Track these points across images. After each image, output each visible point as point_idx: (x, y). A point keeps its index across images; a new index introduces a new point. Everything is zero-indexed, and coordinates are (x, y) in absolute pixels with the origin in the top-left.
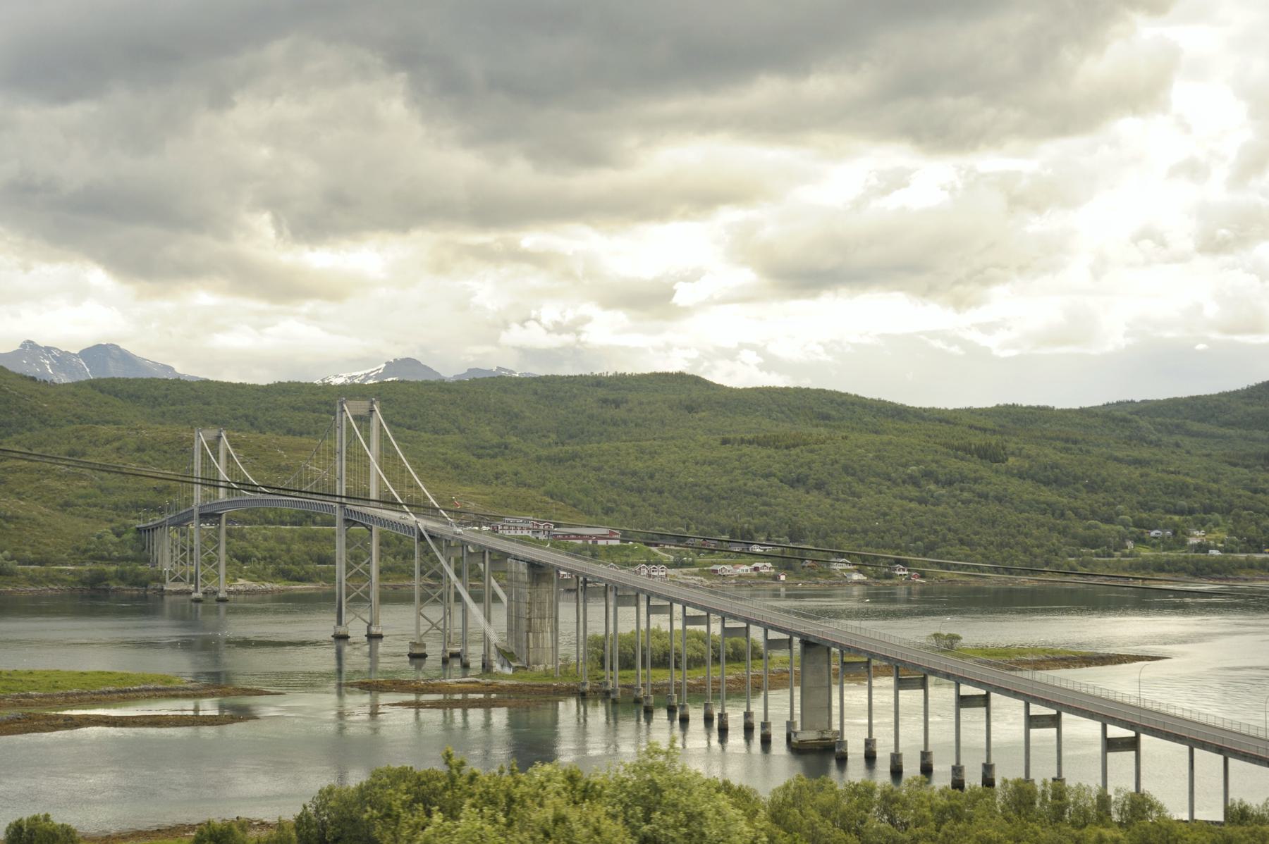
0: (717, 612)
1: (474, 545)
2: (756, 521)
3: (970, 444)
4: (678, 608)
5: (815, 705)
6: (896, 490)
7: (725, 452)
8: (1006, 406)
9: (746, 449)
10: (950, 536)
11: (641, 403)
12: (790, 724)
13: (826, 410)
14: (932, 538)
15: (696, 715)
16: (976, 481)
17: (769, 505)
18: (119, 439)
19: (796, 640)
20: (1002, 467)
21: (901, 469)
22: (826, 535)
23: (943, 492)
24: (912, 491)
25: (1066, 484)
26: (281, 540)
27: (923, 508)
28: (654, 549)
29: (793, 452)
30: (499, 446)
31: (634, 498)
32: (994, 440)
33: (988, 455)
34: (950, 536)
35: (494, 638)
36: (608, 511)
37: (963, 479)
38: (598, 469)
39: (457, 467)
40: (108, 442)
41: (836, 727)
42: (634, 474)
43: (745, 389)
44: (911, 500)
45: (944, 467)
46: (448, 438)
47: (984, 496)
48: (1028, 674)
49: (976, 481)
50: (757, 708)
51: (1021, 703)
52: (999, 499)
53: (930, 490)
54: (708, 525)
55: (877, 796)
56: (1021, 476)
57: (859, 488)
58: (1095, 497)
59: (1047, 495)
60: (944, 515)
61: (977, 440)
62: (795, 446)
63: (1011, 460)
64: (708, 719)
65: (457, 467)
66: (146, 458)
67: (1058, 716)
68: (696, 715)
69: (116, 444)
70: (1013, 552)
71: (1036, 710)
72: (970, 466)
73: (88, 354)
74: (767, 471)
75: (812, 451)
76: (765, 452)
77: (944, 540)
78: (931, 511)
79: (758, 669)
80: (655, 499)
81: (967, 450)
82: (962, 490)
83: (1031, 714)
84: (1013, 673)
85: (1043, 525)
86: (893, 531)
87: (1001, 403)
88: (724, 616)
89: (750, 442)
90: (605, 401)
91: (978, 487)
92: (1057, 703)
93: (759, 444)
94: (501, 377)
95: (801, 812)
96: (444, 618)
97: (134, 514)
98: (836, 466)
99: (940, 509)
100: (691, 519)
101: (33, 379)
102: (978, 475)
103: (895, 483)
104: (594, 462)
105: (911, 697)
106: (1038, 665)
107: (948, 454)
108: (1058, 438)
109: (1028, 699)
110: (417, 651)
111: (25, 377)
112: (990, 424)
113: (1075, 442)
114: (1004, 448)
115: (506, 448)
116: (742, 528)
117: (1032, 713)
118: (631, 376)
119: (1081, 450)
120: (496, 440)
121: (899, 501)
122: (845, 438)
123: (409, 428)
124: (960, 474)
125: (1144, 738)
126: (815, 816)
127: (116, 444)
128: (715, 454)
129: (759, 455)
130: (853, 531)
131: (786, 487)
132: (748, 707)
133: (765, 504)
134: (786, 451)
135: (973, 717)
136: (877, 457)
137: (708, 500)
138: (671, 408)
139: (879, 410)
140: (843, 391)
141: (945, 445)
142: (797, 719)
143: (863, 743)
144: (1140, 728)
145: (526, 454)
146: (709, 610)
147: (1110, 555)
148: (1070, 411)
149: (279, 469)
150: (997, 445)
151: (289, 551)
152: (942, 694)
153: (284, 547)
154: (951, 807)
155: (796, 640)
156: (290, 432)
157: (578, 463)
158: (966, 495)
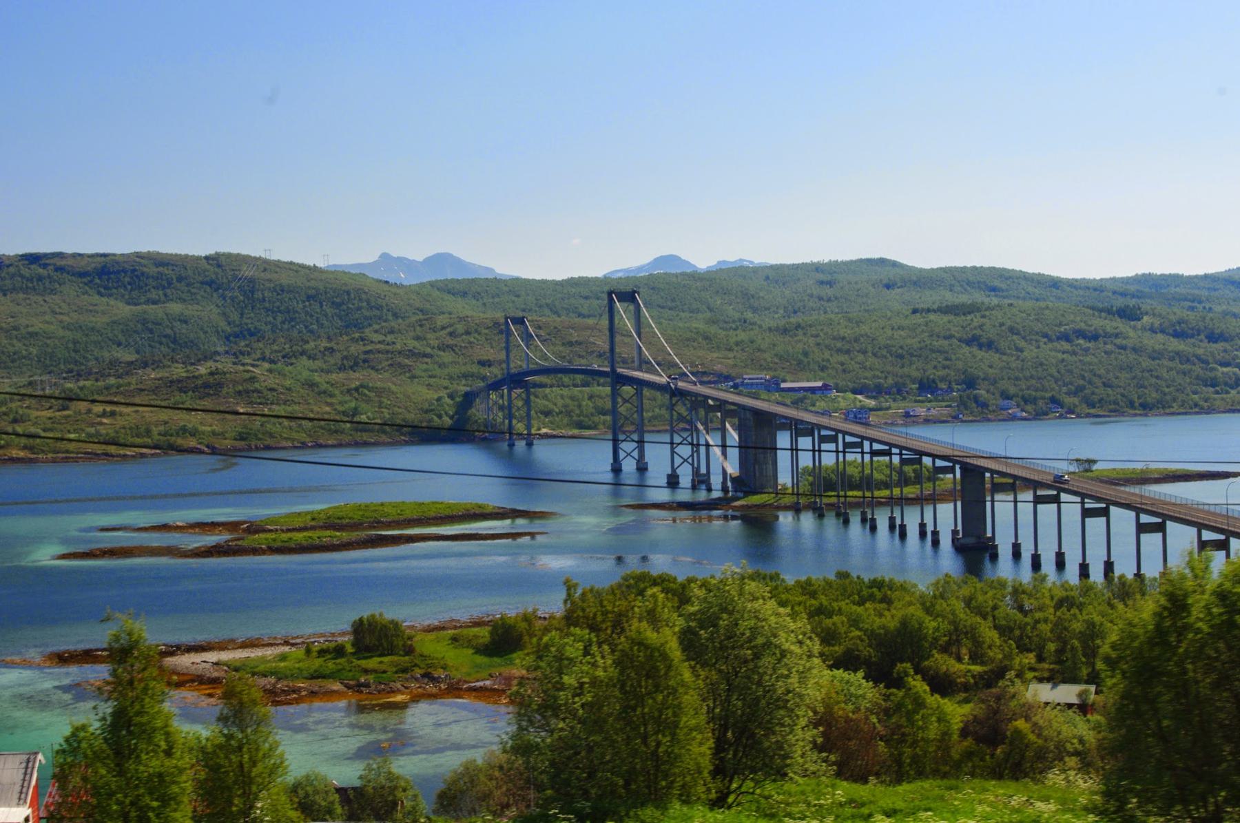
0: (896, 446)
1: (713, 399)
2: (940, 373)
3: (1112, 307)
4: (866, 444)
5: (974, 516)
6: (1050, 345)
7: (918, 319)
8: (1144, 275)
9: (932, 316)
10: (1095, 380)
11: (849, 283)
12: (955, 532)
13: (996, 283)
14: (1081, 382)
15: (855, 519)
16: (1117, 336)
17: (950, 360)
18: (451, 325)
19: (957, 467)
20: (1139, 324)
21: (1057, 328)
22: (996, 382)
23: (1088, 345)
24: (1066, 346)
25: (1192, 336)
26: (572, 398)
27: (1074, 358)
28: (859, 397)
29: (969, 317)
30: (740, 320)
31: (842, 358)
32: (1132, 302)
33: (1129, 314)
34: (1095, 380)
35: (730, 470)
36: (823, 369)
37: (1107, 335)
38: (817, 336)
39: (706, 338)
40: (443, 328)
41: (989, 534)
42: (843, 338)
43: (932, 269)
44: (1063, 353)
45: (1091, 326)
46: (700, 316)
47: (1124, 348)
48: (1135, 490)
49: (1117, 336)
50: (897, 514)
51: (1133, 514)
52: (1134, 350)
53: (1079, 344)
54: (901, 377)
55: (1010, 589)
56: (1152, 330)
57: (1022, 344)
58: (1215, 345)
59: (1175, 345)
60: (1090, 364)
61: (1119, 302)
62: (969, 313)
63: (1145, 318)
64: (864, 520)
65: (706, 338)
66: (472, 339)
67: (1058, 496)
68: (855, 519)
69: (449, 330)
70: (1146, 391)
71: (1145, 519)
72: (1119, 324)
73: (429, 261)
74: (948, 333)
75: (983, 317)
76: (946, 318)
77: (1090, 382)
78: (1080, 361)
79: (928, 488)
80: (860, 357)
81: (1109, 311)
82: (1105, 343)
83: (1203, 539)
84: (1118, 488)
85: (1171, 369)
86: (1049, 378)
87: (1140, 273)
88: (872, 440)
89: (935, 311)
90: (822, 283)
91: (1118, 341)
92: (1162, 514)
93: (941, 312)
94: (741, 267)
95: (306, 327)
96: (692, 456)
97: (464, 382)
98: (1003, 328)
99: (1088, 359)
100: (888, 373)
101: (387, 282)
102: (1118, 331)
103: (1050, 340)
104: (813, 331)
105: (1047, 510)
106: (1158, 481)
107: (1094, 315)
108: (1186, 300)
109: (1139, 511)
110: (673, 480)
111: (381, 281)
112: (1132, 288)
113: (1200, 302)
114: (1140, 309)
115: (745, 322)
116: (928, 378)
117: (1203, 539)
118: (842, 262)
119: (1204, 308)
120: (737, 315)
121: (1053, 353)
122: (1011, 305)
123: (670, 309)
124: (1104, 330)
125: (1112, 508)
126: (959, 606)
127: (449, 330)
128: (907, 322)
129: (941, 320)
130: (1017, 379)
131: (964, 346)
132: (892, 512)
133: (946, 359)
134: (963, 317)
135: (1151, 541)
136: (1037, 320)
137: (901, 357)
138: (873, 285)
139: (1039, 282)
140: (1010, 267)
141: (1093, 308)
142: (960, 527)
143: (1010, 546)
144: (1166, 517)
145: (760, 327)
146: (891, 445)
147: (1227, 392)
148: (1196, 277)
149: (571, 344)
150: (1134, 306)
151: (579, 406)
152: (1071, 508)
153: (576, 403)
154: (1067, 597)
155: (957, 467)
156: (580, 315)
157: (800, 332)
158: (1109, 347)
